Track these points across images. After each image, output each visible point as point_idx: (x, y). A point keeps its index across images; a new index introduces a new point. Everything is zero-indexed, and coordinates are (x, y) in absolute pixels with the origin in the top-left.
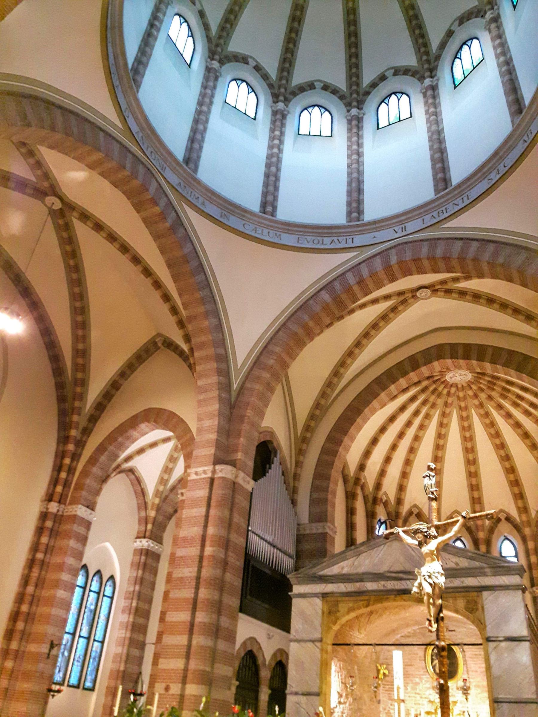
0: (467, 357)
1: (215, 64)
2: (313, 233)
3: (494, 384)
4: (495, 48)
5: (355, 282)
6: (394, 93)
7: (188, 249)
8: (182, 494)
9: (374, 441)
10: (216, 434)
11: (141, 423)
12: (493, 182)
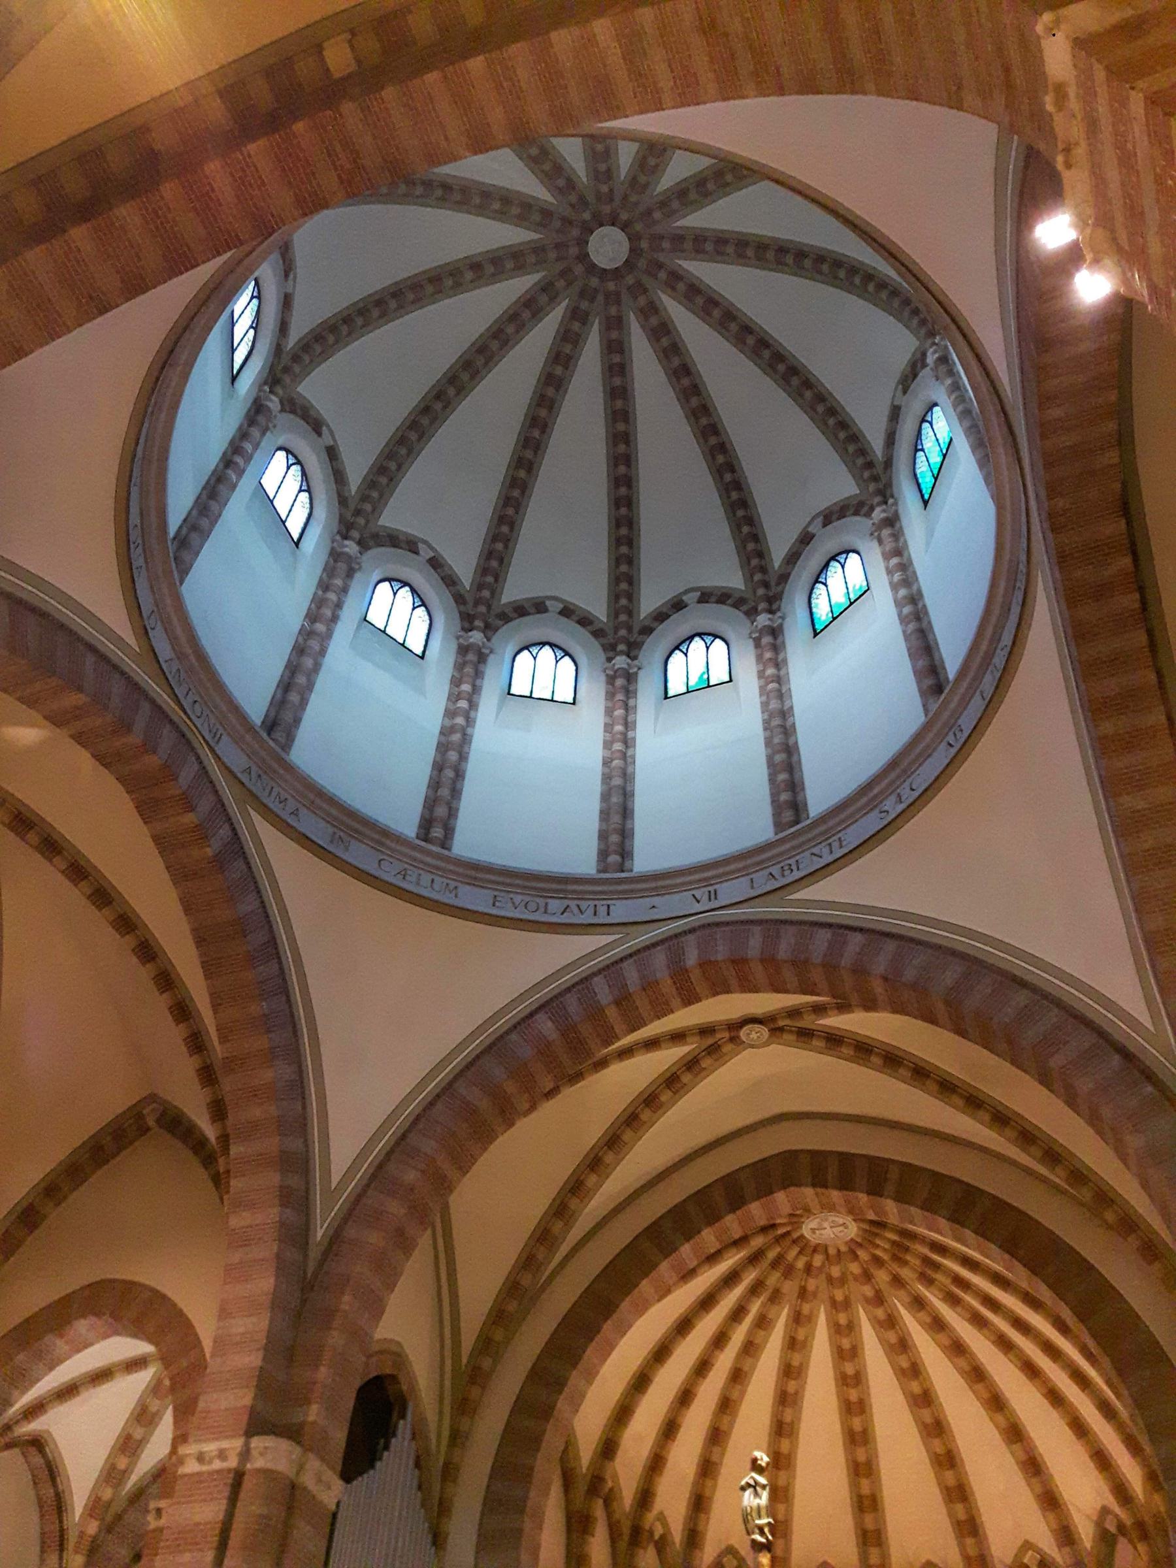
0: (845, 1184)
1: (351, 547)
2: (525, 887)
3: (907, 1249)
4: (889, 572)
5: (610, 998)
6: (700, 635)
7: (247, 905)
8: (159, 1511)
9: (641, 1382)
10: (261, 1354)
11: (76, 1319)
12: (890, 818)
